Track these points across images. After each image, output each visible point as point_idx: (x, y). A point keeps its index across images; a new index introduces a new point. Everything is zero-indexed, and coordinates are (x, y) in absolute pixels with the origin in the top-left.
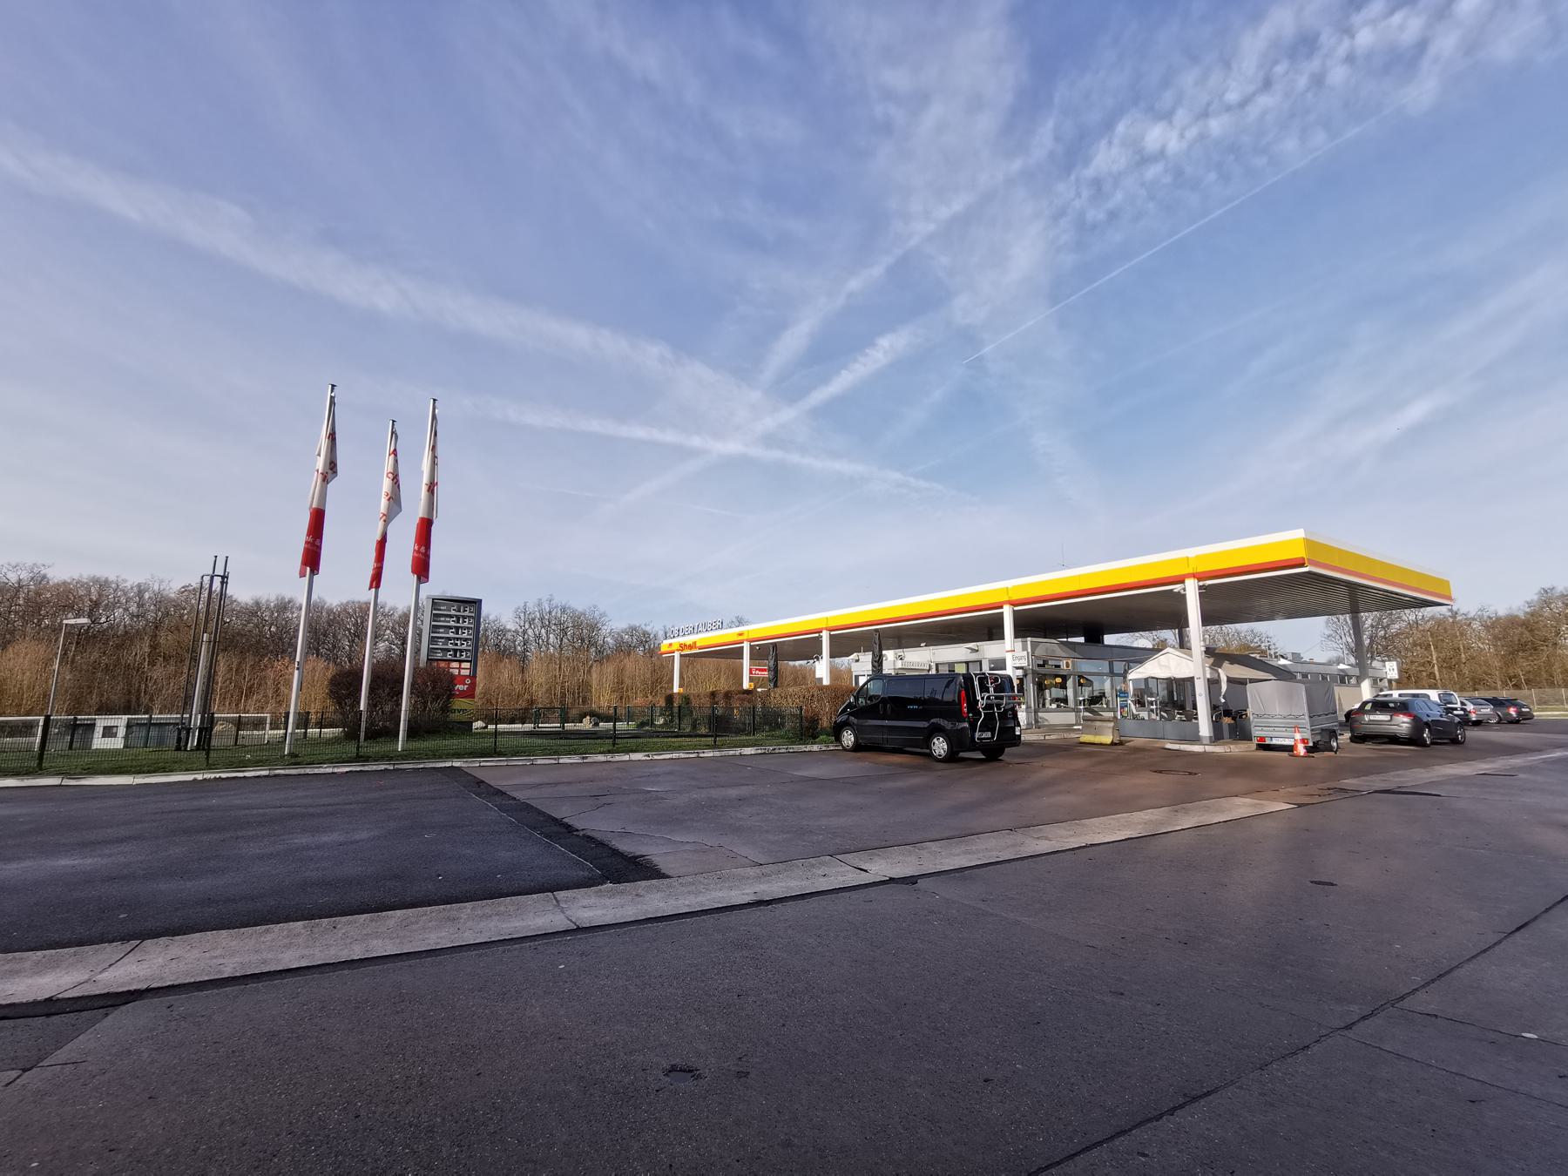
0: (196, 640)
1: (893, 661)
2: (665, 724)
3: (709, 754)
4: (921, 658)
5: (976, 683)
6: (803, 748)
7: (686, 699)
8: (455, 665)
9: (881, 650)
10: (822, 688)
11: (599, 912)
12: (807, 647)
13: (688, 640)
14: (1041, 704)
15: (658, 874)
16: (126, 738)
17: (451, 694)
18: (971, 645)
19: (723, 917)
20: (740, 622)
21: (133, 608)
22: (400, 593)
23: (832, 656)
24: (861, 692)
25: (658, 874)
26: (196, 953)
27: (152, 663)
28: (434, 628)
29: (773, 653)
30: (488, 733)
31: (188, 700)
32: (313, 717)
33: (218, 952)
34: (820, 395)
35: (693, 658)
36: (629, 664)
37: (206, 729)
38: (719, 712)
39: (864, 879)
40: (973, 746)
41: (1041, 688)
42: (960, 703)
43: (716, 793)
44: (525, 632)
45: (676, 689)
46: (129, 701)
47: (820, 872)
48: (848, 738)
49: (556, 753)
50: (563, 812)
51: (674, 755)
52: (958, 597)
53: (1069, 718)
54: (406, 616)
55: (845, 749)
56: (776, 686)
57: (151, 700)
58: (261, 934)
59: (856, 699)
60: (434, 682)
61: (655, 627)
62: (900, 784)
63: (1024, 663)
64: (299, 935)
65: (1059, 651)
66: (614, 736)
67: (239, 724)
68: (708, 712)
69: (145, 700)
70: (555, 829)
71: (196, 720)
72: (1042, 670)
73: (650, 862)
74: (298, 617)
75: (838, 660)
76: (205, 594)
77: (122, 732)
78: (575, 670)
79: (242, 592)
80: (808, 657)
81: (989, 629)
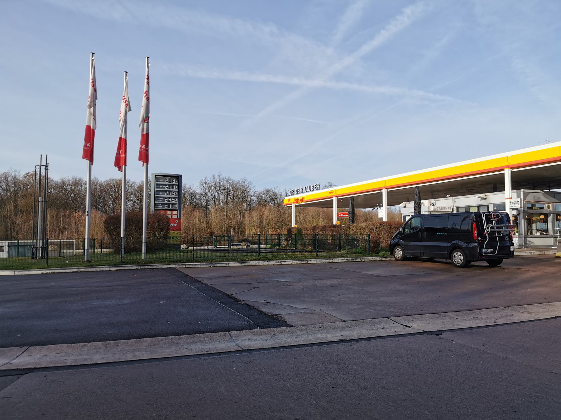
0: (36, 201)
1: (427, 206)
2: (288, 245)
3: (313, 261)
4: (447, 204)
5: (484, 218)
6: (370, 259)
7: (299, 231)
8: (169, 212)
9: (420, 200)
10: (382, 223)
11: (254, 343)
12: (373, 199)
13: (299, 196)
14: (529, 231)
15: (287, 325)
16: (8, 252)
17: (168, 229)
18: (482, 195)
19: (323, 348)
20: (331, 186)
21: (4, 186)
22: (136, 173)
23: (389, 205)
24: (407, 225)
25: (287, 325)
26: (54, 354)
27: (16, 215)
28: (157, 192)
29: (350, 203)
30: (190, 250)
31: (35, 233)
32: (97, 242)
33: (63, 354)
34: (366, 48)
35: (302, 207)
36: (266, 212)
37: (45, 248)
38: (319, 238)
39: (407, 331)
40: (481, 258)
41: (529, 222)
42: (472, 231)
43: (318, 283)
44: (206, 194)
45: (293, 225)
46: (7, 235)
47: (381, 326)
48: (399, 253)
49: (227, 260)
50: (232, 291)
51: (294, 262)
52: (472, 164)
53: (549, 241)
54: (141, 187)
55: (396, 260)
56: (353, 222)
57: (17, 234)
58: (82, 347)
59: (404, 229)
60: (159, 222)
61: (280, 190)
62: (431, 279)
63: (518, 206)
64: (100, 348)
65: (543, 198)
66: (259, 251)
67: (60, 246)
68: (311, 237)
69: (14, 234)
70: (229, 300)
71: (40, 243)
72: (531, 211)
73: (281, 318)
74: (85, 188)
75: (393, 208)
76: (38, 177)
77: (6, 249)
78: (235, 215)
79: (55, 176)
80: (373, 206)
81: (494, 184)
